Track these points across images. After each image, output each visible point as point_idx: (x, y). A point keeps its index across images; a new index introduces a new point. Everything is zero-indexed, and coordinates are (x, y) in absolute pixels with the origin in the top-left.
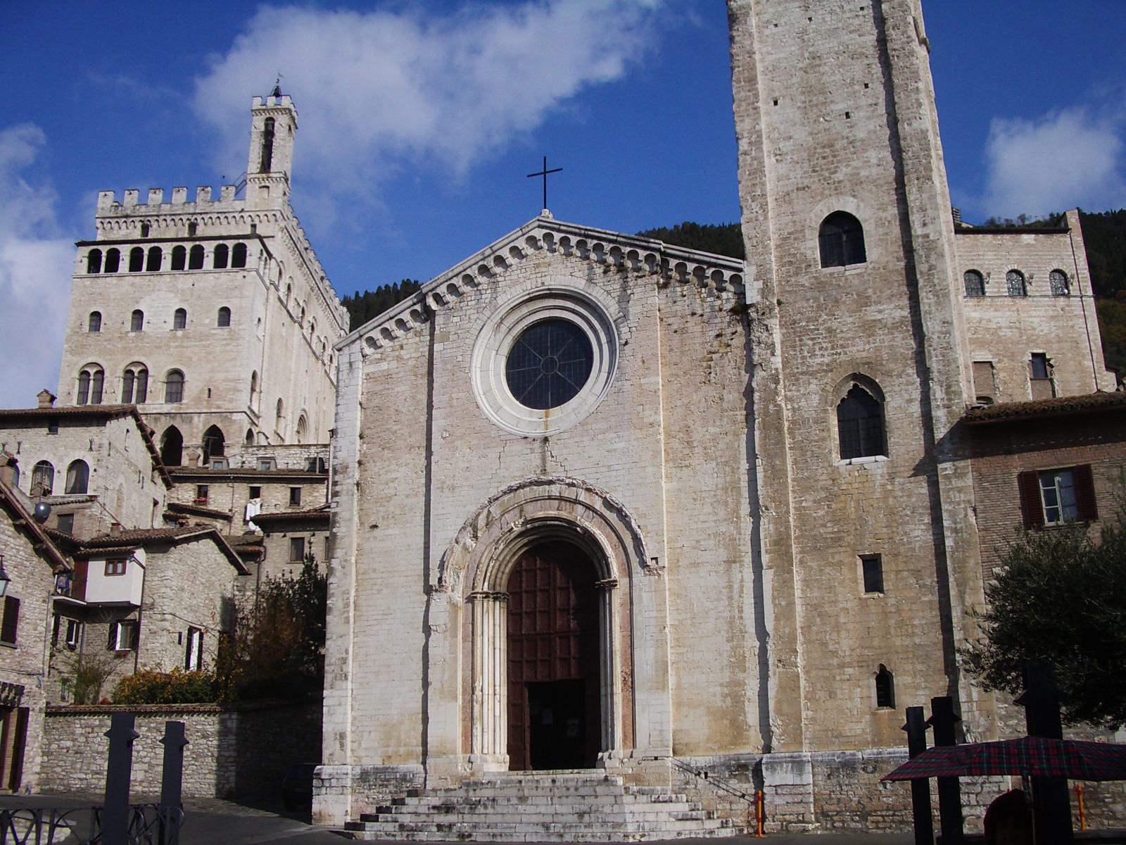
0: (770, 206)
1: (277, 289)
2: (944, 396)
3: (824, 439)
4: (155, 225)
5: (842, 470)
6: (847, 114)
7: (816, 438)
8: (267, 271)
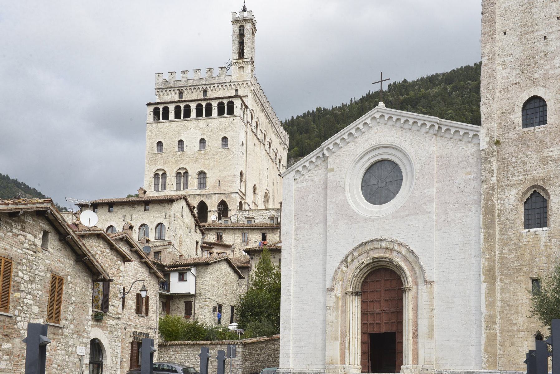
0: (497, 95)
1: (251, 126)
3: (516, 219)
4: (186, 92)
5: (524, 235)
6: (545, 37)
7: (512, 219)
8: (245, 116)
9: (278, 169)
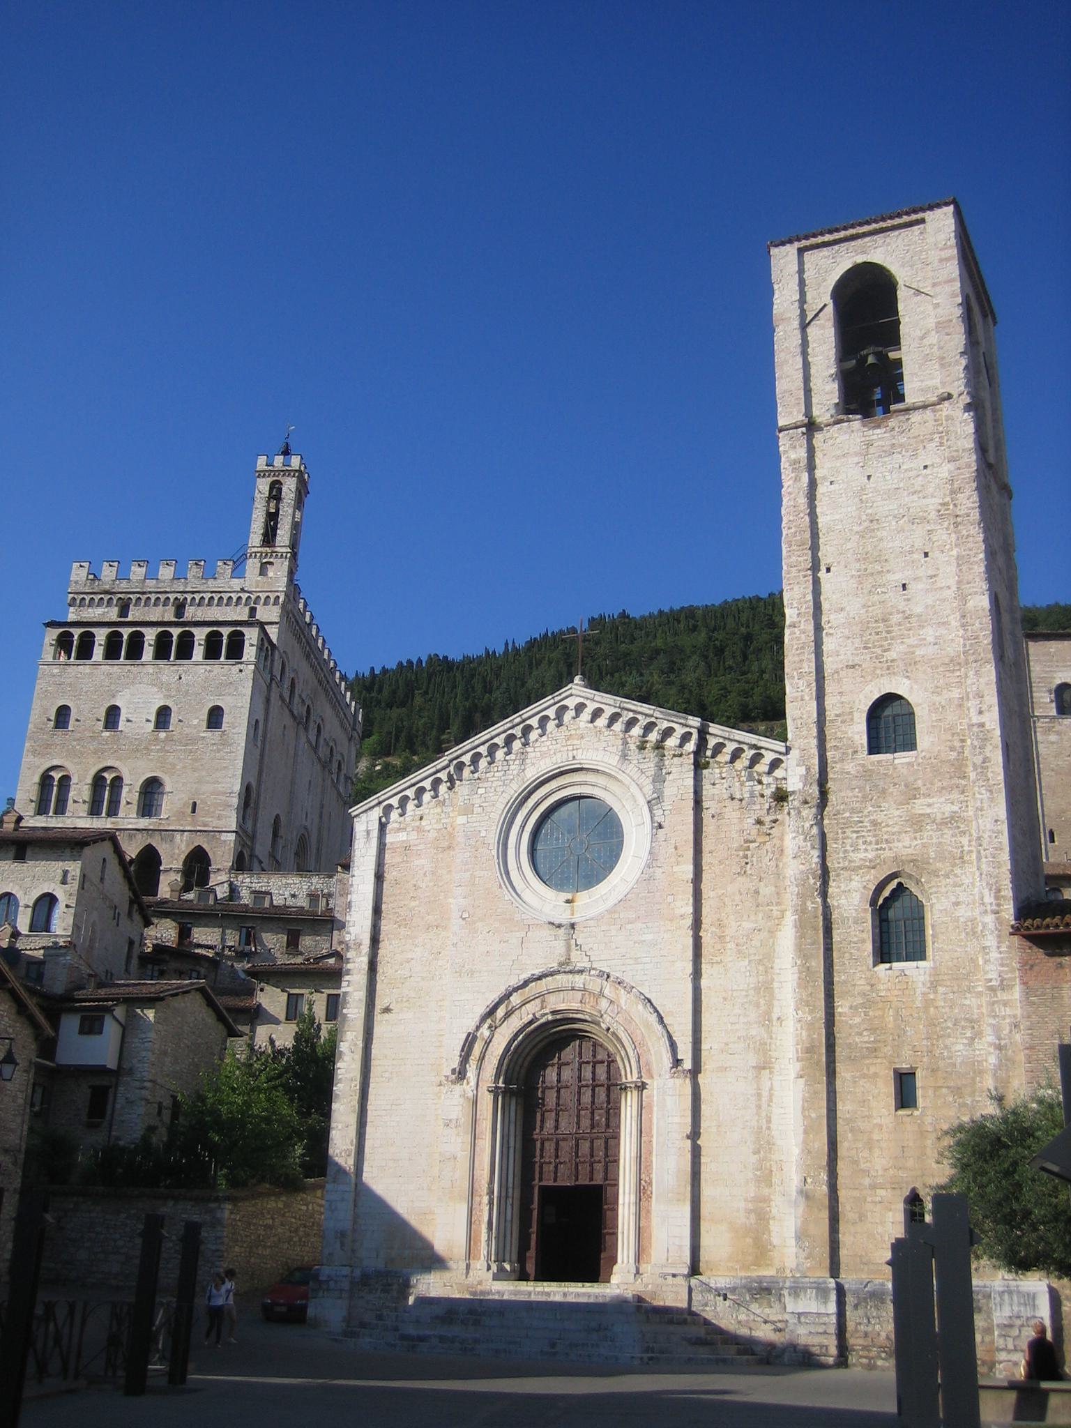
2: (992, 900)
6: (904, 585)
9: (335, 785)
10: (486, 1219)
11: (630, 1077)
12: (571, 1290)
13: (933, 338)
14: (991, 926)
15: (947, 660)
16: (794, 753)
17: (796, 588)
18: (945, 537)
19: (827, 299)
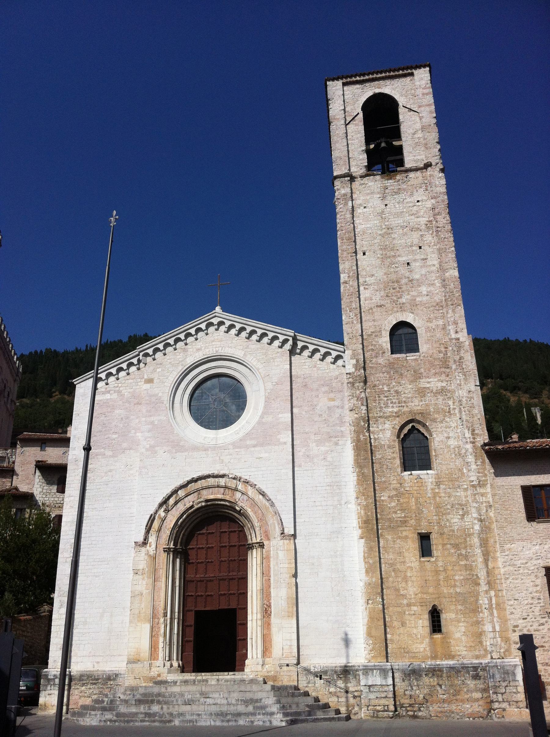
2: (470, 435)
6: (408, 264)
7: (389, 457)
10: (162, 631)
11: (254, 539)
12: (220, 677)
13: (420, 134)
14: (471, 450)
15: (435, 304)
16: (348, 353)
17: (347, 263)
18: (430, 239)
19: (359, 110)
